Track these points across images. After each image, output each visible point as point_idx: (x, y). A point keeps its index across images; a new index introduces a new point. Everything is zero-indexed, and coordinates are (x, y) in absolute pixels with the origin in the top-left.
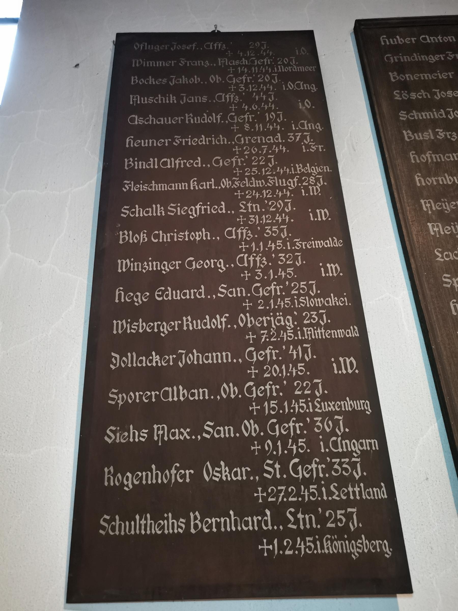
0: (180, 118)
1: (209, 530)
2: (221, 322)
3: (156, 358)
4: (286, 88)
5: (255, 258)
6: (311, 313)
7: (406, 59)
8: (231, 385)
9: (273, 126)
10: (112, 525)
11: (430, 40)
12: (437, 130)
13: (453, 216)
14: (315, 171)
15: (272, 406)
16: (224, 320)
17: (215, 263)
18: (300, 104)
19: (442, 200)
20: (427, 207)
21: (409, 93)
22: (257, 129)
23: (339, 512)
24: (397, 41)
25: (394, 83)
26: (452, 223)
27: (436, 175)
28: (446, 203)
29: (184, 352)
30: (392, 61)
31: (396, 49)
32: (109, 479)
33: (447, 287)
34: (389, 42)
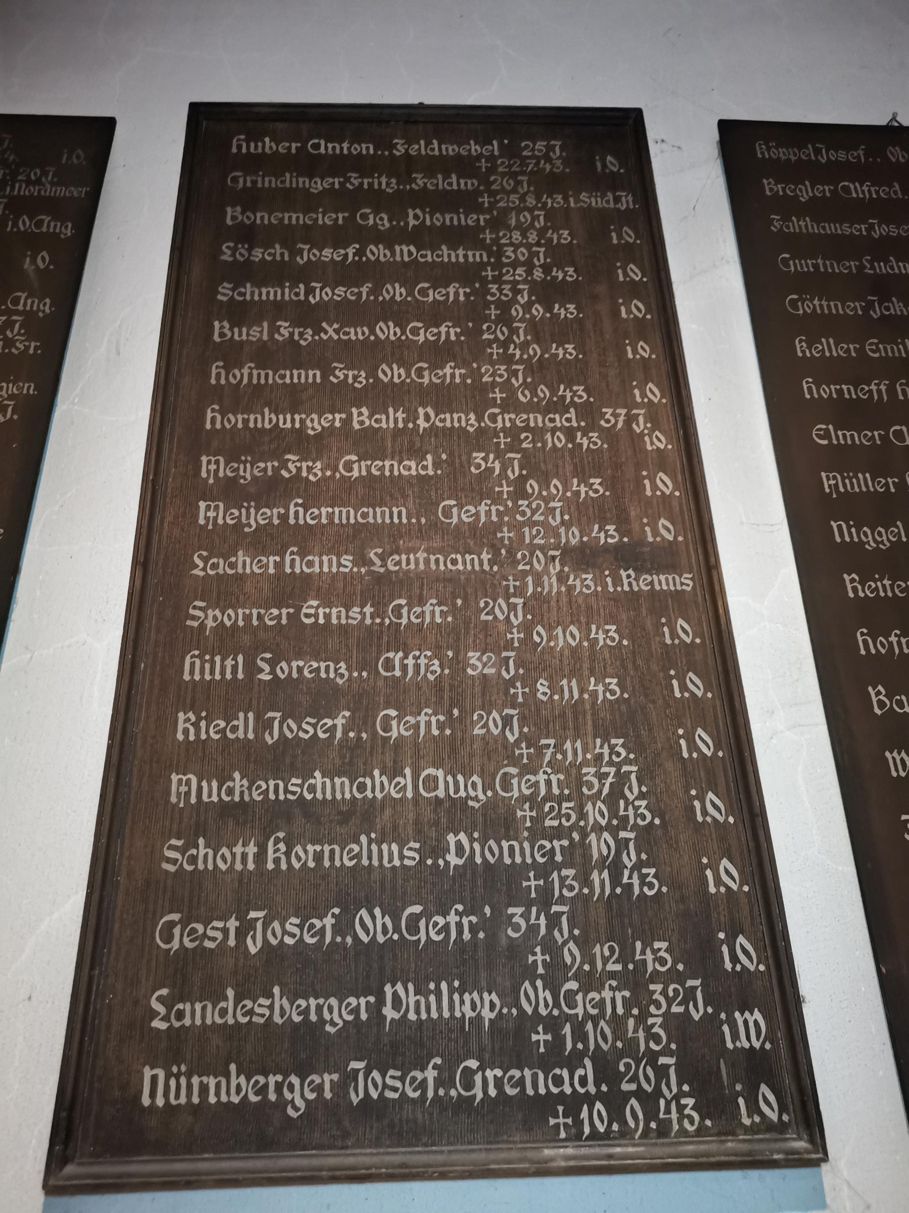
1: (259, 1098)
3: (238, 782)
4: (12, 227)
7: (267, 182)
11: (326, 148)
12: (279, 323)
13: (252, 490)
18: (28, 259)
19: (243, 458)
20: (208, 471)
21: (250, 250)
23: (565, 805)
24: (264, 147)
25: (229, 227)
26: (245, 504)
27: (248, 410)
28: (248, 465)
30: (241, 185)
31: (254, 163)
33: (193, 627)
34: (248, 147)
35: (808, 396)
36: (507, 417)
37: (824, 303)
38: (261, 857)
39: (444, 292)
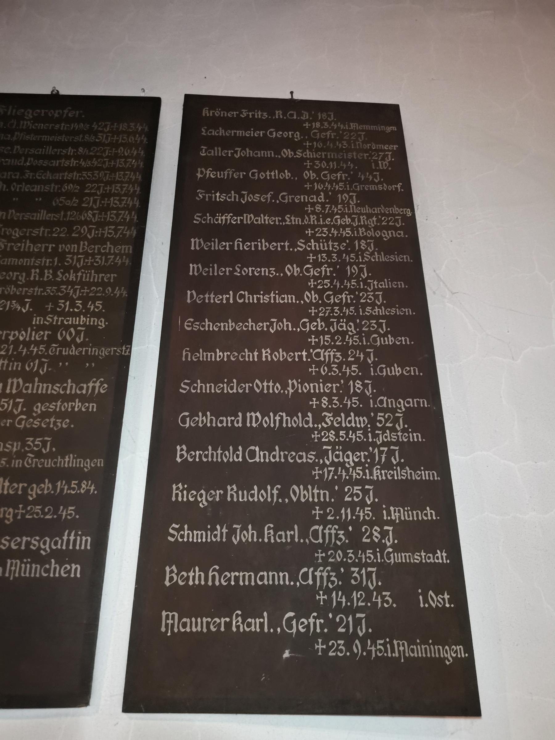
2: (272, 495)
5: (337, 532)
8: (295, 266)
9: (365, 175)
10: (181, 534)
15: (326, 339)
16: (275, 492)
17: (293, 135)
32: (177, 495)
36: (290, 197)
38: (260, 356)
39: (335, 175)
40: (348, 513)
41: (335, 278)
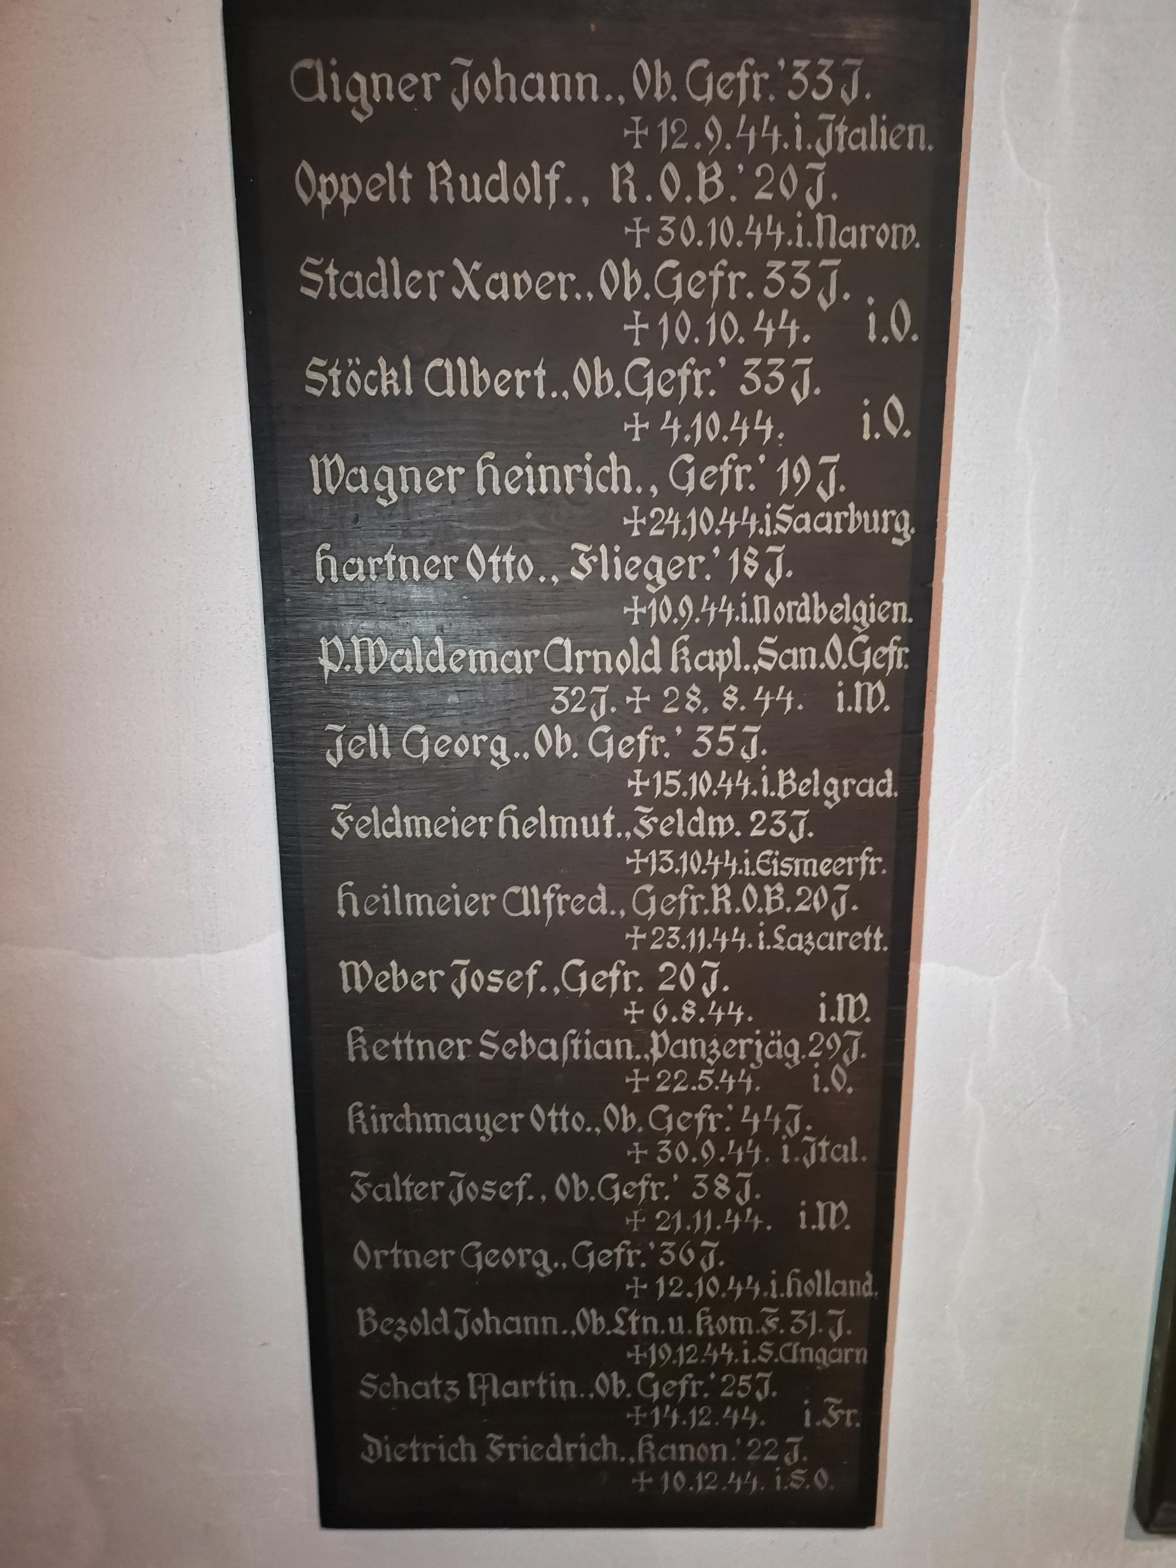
0: (485, 898)
2: (545, 185)
6: (671, 929)
14: (863, 619)
15: (668, 782)
16: (553, 177)
22: (698, 1226)
29: (462, 1175)
35: (342, 913)
37: (409, 1041)
40: (706, 1218)
41: (729, 1136)
